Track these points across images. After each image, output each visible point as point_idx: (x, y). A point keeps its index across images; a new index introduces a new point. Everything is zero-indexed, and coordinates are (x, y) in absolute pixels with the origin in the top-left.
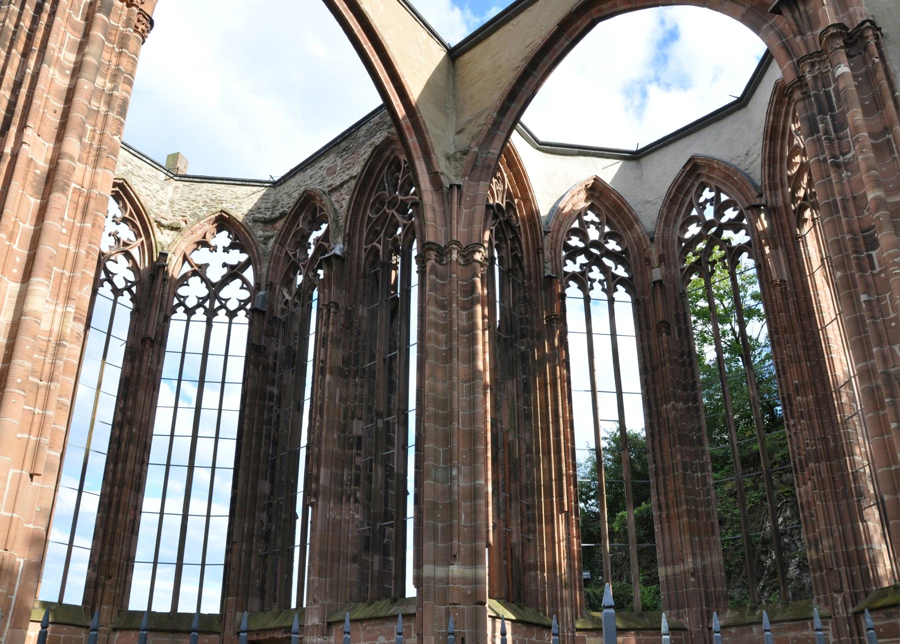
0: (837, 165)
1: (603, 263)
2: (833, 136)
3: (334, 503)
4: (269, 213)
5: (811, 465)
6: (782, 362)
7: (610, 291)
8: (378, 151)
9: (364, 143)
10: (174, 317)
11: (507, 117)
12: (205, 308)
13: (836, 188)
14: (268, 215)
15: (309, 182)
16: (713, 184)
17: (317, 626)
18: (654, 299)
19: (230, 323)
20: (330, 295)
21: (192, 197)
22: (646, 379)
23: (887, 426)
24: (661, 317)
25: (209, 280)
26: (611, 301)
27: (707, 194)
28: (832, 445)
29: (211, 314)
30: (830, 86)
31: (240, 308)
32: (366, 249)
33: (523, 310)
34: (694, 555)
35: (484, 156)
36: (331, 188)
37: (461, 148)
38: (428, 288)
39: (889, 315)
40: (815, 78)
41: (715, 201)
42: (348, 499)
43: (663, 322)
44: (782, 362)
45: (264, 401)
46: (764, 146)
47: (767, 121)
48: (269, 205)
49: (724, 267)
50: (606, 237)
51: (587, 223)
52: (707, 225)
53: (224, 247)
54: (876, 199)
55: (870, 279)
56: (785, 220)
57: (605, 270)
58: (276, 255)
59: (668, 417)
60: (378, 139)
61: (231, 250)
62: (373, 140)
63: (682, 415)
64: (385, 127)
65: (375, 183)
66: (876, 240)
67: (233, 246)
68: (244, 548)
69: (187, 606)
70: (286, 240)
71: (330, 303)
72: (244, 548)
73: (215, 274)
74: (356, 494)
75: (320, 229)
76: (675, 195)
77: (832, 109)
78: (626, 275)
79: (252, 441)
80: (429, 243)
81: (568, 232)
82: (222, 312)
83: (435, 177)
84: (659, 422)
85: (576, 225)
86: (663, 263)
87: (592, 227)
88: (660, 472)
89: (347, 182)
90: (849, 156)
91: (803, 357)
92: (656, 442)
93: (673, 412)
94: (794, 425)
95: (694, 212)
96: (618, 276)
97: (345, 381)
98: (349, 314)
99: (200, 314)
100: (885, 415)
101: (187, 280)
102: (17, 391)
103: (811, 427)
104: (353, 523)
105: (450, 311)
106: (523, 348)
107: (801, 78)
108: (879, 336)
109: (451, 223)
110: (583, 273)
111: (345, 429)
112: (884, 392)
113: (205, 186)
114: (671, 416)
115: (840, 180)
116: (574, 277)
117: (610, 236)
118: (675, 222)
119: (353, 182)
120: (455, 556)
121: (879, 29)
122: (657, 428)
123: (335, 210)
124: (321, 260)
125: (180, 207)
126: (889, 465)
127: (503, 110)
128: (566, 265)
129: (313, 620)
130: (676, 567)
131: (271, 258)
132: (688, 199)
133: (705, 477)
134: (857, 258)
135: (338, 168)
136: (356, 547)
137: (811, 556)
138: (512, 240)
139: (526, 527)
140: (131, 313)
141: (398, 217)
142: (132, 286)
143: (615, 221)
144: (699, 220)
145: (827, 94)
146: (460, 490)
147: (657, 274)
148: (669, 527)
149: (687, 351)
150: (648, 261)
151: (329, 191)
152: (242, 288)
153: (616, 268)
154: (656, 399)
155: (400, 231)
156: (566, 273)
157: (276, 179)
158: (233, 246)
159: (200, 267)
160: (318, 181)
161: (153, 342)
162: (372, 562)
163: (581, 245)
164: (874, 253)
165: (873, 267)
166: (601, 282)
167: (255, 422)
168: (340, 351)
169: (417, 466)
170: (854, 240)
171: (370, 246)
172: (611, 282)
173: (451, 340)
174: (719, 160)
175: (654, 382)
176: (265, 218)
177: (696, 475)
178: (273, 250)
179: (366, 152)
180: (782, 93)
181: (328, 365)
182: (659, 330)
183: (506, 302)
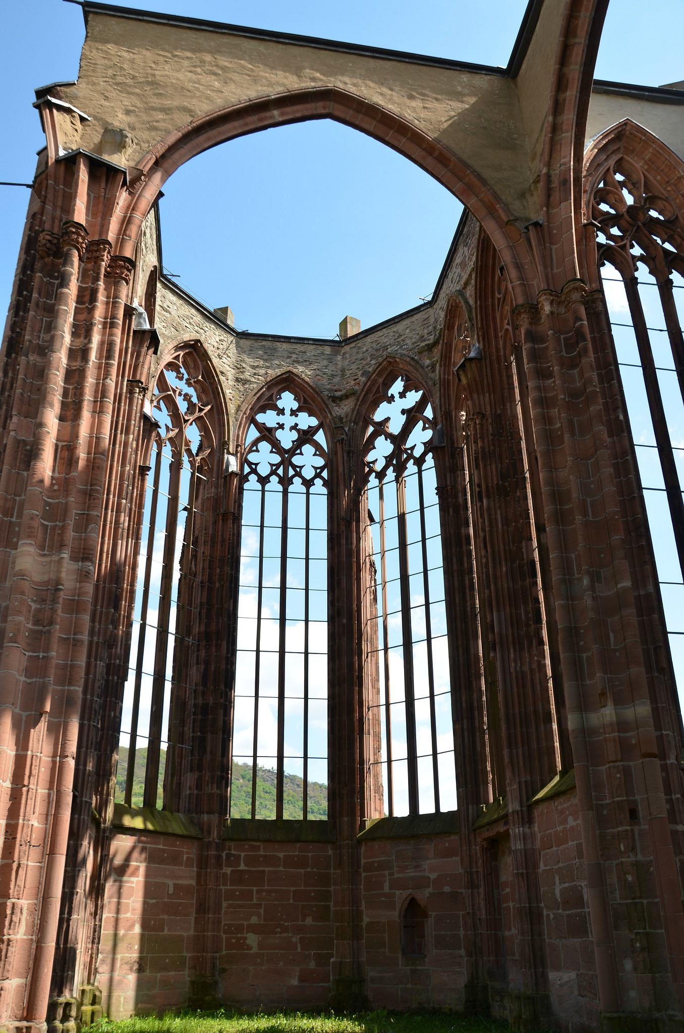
4: (432, 337)
11: (566, 112)
17: (518, 811)
21: (360, 356)
29: (286, 482)
58: (444, 379)
67: (407, 389)
68: (465, 726)
69: (426, 807)
72: (465, 726)
73: (287, 439)
78: (620, 234)
82: (297, 481)
99: (390, 474)
102: (10, 644)
113: (369, 339)
124: (457, 371)
125: (351, 372)
131: (440, 385)
142: (321, 472)
157: (429, 298)
158: (407, 389)
167: (455, 574)
171: (181, 365)
181: (483, 487)
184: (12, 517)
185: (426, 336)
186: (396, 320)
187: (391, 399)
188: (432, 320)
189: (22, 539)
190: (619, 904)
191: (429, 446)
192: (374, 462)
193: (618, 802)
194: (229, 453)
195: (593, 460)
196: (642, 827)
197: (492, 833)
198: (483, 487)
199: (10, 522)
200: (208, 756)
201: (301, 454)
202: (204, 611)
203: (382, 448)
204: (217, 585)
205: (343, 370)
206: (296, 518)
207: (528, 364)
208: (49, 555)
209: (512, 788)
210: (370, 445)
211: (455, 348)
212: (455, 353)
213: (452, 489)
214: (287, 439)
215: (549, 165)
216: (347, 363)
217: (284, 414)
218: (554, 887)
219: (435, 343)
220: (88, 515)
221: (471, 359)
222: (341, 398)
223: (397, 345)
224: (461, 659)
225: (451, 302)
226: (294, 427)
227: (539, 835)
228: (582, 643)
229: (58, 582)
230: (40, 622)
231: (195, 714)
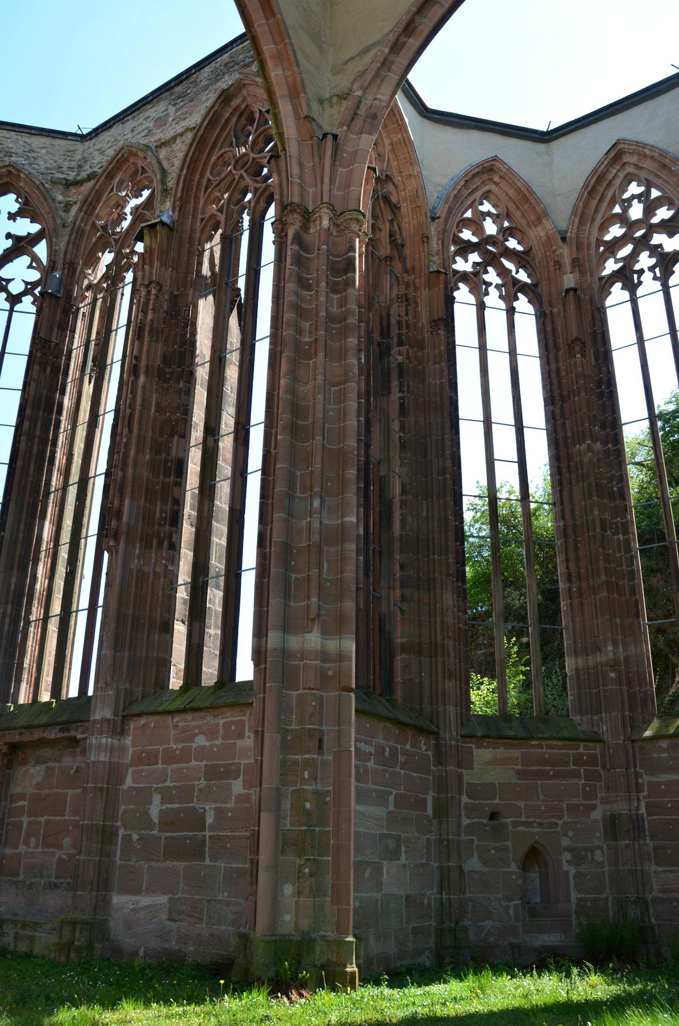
3: (141, 548)
4: (73, 174)
7: (509, 299)
8: (225, 97)
11: (401, 55)
14: (71, 176)
15: (130, 135)
16: (643, 174)
17: (109, 720)
18: (565, 311)
19: (11, 311)
20: (151, 274)
22: (553, 411)
24: (574, 333)
27: (634, 189)
32: (202, 219)
34: (615, 644)
35: (369, 103)
36: (159, 143)
37: (337, 91)
41: (643, 197)
42: (160, 545)
43: (577, 339)
48: (74, 164)
49: (655, 278)
50: (507, 233)
51: (482, 213)
52: (632, 226)
53: (9, 213)
57: (656, 250)
58: (80, 226)
60: (226, 82)
61: (18, 218)
62: (219, 84)
63: (599, 460)
64: (236, 67)
68: (9, 612)
70: (94, 208)
71: (151, 283)
72: (9, 612)
74: (171, 537)
75: (141, 196)
79: (29, 465)
84: (569, 467)
85: (468, 214)
86: (577, 269)
89: (182, 134)
92: (565, 493)
95: (617, 209)
96: (519, 281)
97: (165, 385)
104: (165, 577)
105: (317, 291)
109: (322, 183)
110: (476, 274)
114: (586, 460)
116: (464, 277)
118: (593, 220)
119: (189, 136)
122: (568, 475)
123: (163, 169)
124: (142, 228)
128: (455, 262)
129: (101, 713)
130: (590, 658)
131: (73, 229)
135: (170, 119)
138: (391, 222)
141: (248, 180)
143: (518, 214)
144: (623, 219)
147: (569, 280)
148: (582, 604)
150: (558, 264)
151: (156, 147)
152: (30, 267)
153: (517, 272)
154: (566, 438)
155: (249, 196)
156: (456, 272)
157: (85, 132)
158: (20, 213)
160: (143, 134)
163: (475, 240)
166: (498, 287)
167: (36, 440)
169: (264, 495)
173: (316, 329)
174: (652, 146)
175: (563, 416)
176: (67, 180)
177: (616, 537)
178: (76, 220)
179: (208, 99)
185: (65, 169)
186: (33, 132)
188: (78, 156)
190: (288, 830)
191: (29, 288)
193: (309, 730)
195: (336, 388)
196: (325, 758)
197: (17, 738)
207: (291, 265)
209: (107, 693)
211: (106, 201)
212: (102, 206)
213: (55, 346)
218: (148, 806)
219: (78, 183)
221: (163, 223)
223: (25, 160)
224: (21, 535)
225: (123, 151)
227: (131, 750)
228: (293, 563)
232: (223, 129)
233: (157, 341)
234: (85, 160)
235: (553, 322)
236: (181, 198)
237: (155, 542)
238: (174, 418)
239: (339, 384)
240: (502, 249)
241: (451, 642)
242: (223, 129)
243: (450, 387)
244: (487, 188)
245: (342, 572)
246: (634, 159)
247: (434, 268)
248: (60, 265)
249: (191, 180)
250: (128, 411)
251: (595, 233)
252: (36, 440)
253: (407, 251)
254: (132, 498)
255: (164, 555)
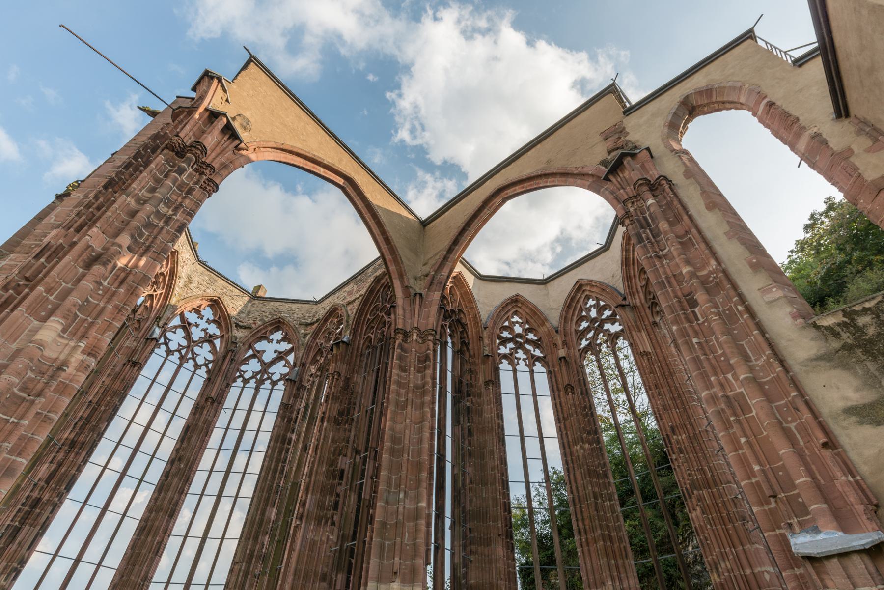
0: (659, 257)
1: (525, 348)
2: (653, 240)
5: (695, 492)
6: (658, 411)
7: (531, 366)
8: (378, 280)
9: (370, 276)
10: (234, 384)
12: (256, 379)
13: (661, 270)
14: (309, 321)
16: (594, 295)
21: (263, 310)
23: (738, 442)
25: (263, 361)
26: (532, 372)
27: (591, 302)
28: (709, 475)
29: (183, 359)
30: (646, 213)
31: (280, 380)
33: (469, 378)
37: (424, 273)
38: (395, 358)
39: (717, 352)
40: (635, 210)
41: (597, 306)
43: (568, 385)
44: (658, 411)
45: (284, 444)
46: (622, 270)
47: (622, 255)
49: (608, 347)
51: (513, 322)
52: (593, 321)
54: (688, 272)
55: (697, 328)
56: (643, 314)
57: (526, 352)
59: (578, 456)
65: (374, 298)
66: (696, 300)
67: (283, 340)
70: (318, 335)
76: (570, 304)
77: (649, 225)
78: (541, 355)
80: (398, 329)
81: (501, 328)
82: (191, 362)
83: (406, 288)
85: (507, 324)
87: (517, 325)
88: (577, 501)
89: (358, 298)
90: (665, 251)
91: (672, 406)
93: (582, 451)
94: (676, 459)
95: (584, 314)
98: (347, 380)
99: (252, 383)
100: (734, 433)
101: (248, 361)
103: (688, 461)
104: (327, 543)
106: (468, 404)
107: (627, 212)
108: (714, 368)
110: (511, 354)
111: (332, 463)
112: (728, 412)
113: (272, 303)
114: (580, 455)
115: (663, 266)
116: (505, 356)
117: (530, 330)
118: (572, 320)
119: (361, 298)
120: (396, 573)
121: (671, 181)
126: (750, 478)
127: (450, 250)
128: (499, 349)
132: (579, 306)
133: (613, 504)
134: (684, 314)
136: (327, 566)
137: (714, 579)
139: (468, 549)
140: (205, 381)
143: (532, 321)
145: (645, 218)
146: (406, 511)
147: (562, 353)
148: (589, 550)
149: (588, 405)
150: (555, 345)
153: (534, 351)
154: (568, 442)
156: (499, 354)
157: (318, 300)
158: (283, 340)
159: (259, 352)
161: (213, 401)
162: (336, 580)
163: (510, 336)
164: (696, 310)
165: (697, 319)
166: (524, 360)
167: (274, 460)
168: (337, 405)
170: (680, 301)
172: (532, 360)
180: (627, 238)
181: (327, 415)
182: (566, 390)
183: (456, 372)
184: (51, 296)
187: (271, 341)
188: (314, 311)
189: (56, 316)
191: (283, 377)
192: (244, 372)
194: (158, 326)
198: (327, 415)
199: (48, 299)
200: (14, 547)
201: (201, 347)
202: (80, 424)
203: (253, 366)
204: (103, 408)
205: (249, 312)
206: (179, 385)
208: (67, 339)
210: (246, 361)
214: (197, 334)
215: (436, 272)
216: (253, 309)
217: (202, 319)
219: (312, 324)
220: (110, 323)
221: (343, 342)
222: (241, 327)
224: (258, 518)
226: (205, 330)
229: (65, 363)
230: (28, 390)
231: (23, 505)
232: (376, 294)
233: (335, 403)
234: (316, 313)
235: (555, 376)
236: (354, 329)
237: (323, 521)
238: (341, 445)
239: (419, 423)
240: (525, 340)
241: (503, 582)
242: (376, 294)
243: (498, 417)
244: (515, 309)
245: (416, 539)
246: (588, 288)
247: (486, 353)
248: (298, 364)
249: (360, 320)
250: (316, 443)
251: (574, 327)
252: (274, 460)
253: (471, 346)
254: (312, 495)
255: (328, 529)
